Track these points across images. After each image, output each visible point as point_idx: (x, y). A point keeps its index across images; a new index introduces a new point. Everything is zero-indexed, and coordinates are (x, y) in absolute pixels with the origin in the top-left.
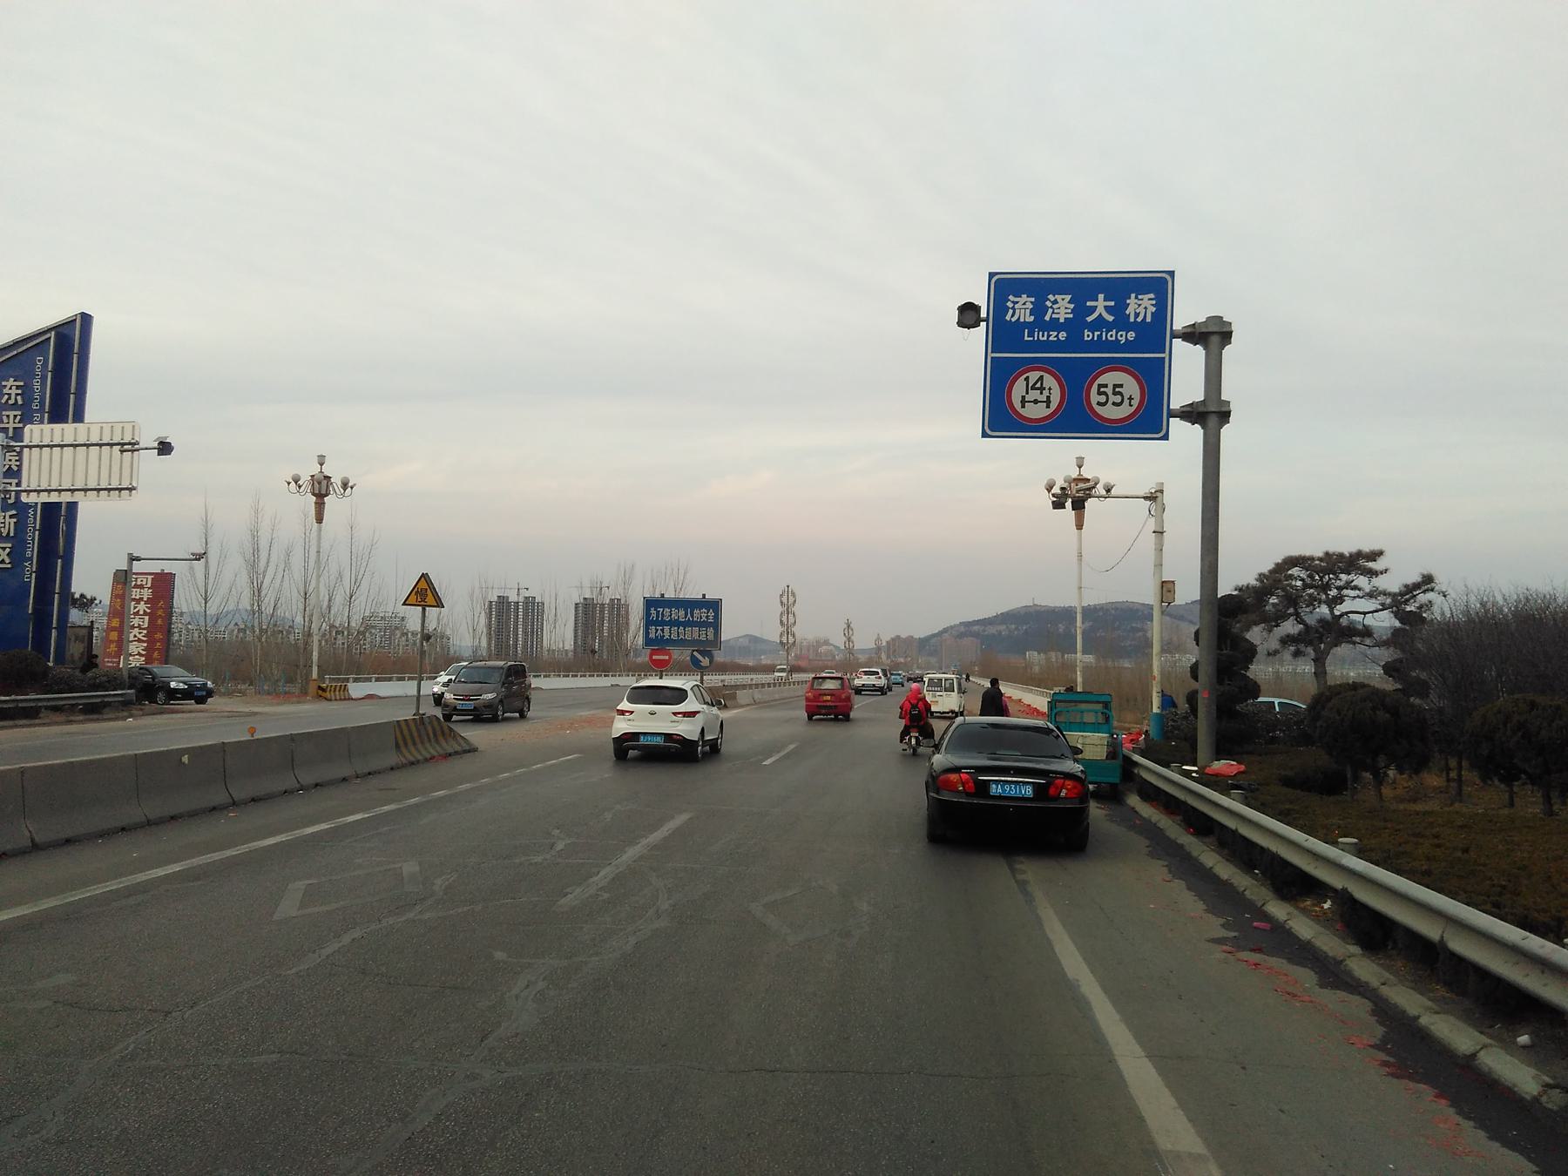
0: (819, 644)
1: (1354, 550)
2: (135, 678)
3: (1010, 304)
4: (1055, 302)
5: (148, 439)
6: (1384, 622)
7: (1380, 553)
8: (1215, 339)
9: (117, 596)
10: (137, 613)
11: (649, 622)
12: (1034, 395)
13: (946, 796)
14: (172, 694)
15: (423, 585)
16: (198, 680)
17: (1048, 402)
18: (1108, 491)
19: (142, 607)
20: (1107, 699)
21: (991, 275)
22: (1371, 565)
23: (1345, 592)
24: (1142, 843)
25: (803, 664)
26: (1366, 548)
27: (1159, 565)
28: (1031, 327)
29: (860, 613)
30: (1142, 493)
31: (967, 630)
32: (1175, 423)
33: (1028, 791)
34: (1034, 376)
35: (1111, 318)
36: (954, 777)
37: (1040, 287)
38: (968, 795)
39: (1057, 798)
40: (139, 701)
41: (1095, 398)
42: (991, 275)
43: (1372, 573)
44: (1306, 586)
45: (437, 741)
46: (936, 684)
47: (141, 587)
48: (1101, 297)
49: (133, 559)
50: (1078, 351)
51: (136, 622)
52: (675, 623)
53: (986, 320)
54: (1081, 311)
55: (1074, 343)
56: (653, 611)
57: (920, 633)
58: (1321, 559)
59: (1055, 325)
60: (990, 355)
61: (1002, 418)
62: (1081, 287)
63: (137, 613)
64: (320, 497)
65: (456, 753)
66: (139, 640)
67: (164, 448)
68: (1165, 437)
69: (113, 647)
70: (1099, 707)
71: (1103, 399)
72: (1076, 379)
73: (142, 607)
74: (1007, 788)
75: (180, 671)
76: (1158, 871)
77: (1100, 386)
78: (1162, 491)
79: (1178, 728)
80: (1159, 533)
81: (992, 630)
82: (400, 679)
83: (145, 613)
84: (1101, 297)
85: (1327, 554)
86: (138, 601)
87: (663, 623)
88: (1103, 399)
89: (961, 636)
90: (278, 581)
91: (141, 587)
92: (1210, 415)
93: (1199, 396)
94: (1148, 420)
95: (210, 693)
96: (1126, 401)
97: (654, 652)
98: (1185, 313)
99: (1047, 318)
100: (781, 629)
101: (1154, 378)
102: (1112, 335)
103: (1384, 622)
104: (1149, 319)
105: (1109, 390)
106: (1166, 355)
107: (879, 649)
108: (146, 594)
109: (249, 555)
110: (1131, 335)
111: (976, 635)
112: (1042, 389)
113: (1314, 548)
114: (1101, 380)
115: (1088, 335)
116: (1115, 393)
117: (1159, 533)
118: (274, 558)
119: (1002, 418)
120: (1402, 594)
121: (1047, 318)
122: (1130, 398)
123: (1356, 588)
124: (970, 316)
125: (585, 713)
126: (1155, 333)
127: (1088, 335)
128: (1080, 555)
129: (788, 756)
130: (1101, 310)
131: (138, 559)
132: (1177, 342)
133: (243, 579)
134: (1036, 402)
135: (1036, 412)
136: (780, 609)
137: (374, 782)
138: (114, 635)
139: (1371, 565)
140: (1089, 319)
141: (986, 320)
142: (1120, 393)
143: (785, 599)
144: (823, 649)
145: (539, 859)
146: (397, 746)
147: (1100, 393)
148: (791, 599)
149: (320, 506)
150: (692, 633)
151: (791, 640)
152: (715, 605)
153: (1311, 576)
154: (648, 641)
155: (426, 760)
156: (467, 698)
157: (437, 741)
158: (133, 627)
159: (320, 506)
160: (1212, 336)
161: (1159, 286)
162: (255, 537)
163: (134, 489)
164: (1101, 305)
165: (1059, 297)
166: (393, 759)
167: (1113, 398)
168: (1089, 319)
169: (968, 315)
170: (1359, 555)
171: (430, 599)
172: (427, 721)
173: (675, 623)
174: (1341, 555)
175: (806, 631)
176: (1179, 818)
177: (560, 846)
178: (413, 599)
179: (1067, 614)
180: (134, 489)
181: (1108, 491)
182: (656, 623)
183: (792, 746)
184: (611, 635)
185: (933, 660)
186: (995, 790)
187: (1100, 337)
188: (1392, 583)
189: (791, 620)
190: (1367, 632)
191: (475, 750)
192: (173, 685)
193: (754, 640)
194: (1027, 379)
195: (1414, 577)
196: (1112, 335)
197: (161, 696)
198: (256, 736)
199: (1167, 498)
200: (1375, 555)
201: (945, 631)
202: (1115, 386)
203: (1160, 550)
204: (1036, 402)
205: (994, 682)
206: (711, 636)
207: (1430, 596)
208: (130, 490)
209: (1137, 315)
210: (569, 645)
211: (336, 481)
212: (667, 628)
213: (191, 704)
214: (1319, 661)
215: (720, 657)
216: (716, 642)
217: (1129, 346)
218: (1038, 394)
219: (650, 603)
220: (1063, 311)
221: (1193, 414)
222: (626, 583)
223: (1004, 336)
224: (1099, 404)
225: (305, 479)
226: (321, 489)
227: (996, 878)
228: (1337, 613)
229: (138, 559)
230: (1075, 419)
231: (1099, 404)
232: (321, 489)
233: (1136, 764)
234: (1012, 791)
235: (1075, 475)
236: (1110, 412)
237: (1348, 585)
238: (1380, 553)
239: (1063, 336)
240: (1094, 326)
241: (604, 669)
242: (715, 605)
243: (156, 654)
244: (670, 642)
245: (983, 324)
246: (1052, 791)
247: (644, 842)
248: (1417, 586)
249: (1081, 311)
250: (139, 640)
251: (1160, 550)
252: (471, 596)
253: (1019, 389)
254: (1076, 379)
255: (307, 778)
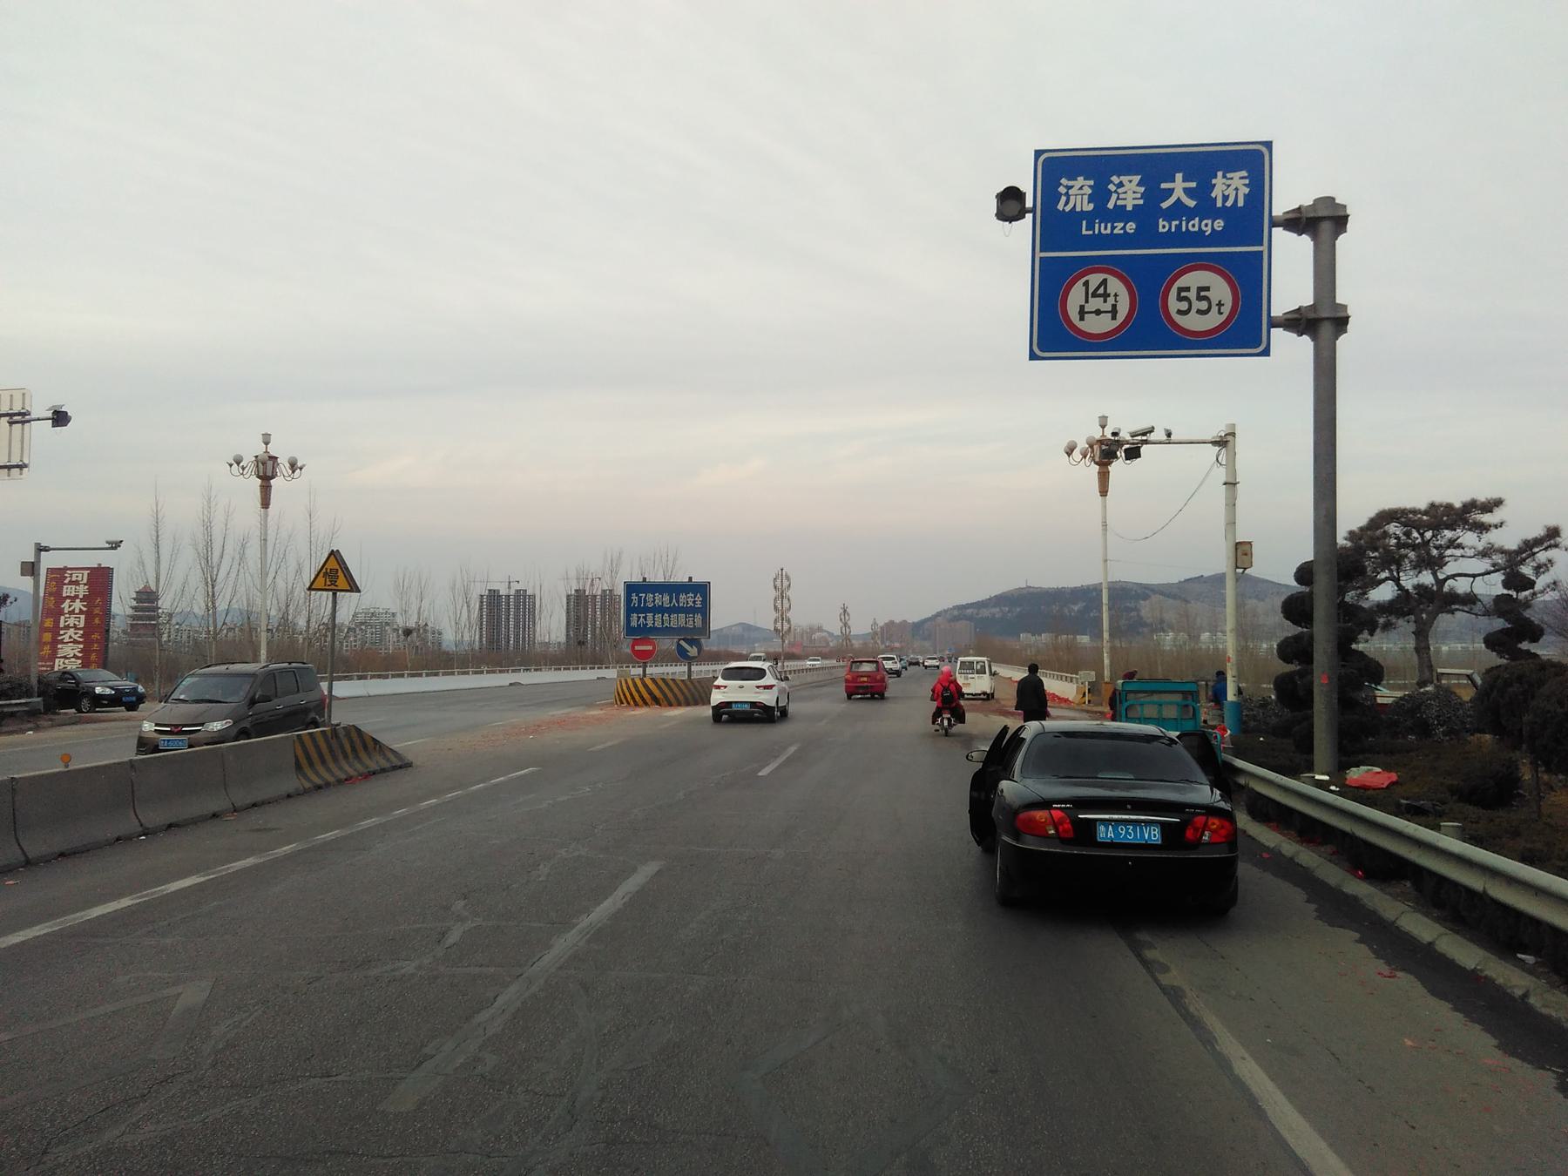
0: (812, 630)
1: (1467, 498)
2: (48, 684)
3: (1062, 190)
4: (1121, 185)
5: (40, 409)
6: (1492, 587)
7: (1498, 503)
8: (1326, 227)
9: (51, 594)
10: (72, 612)
11: (630, 610)
12: (1096, 303)
13: (1030, 844)
14: (98, 701)
15: (333, 564)
16: (126, 684)
17: (1114, 312)
18: (1169, 435)
19: (78, 605)
20: (1192, 687)
21: (1038, 153)
22: (1486, 518)
23: (1449, 552)
24: (1297, 895)
25: (795, 650)
26: (1482, 497)
27: (1231, 523)
28: (1090, 217)
29: (858, 598)
30: (1210, 438)
31: (960, 613)
32: (1278, 334)
33: (1153, 835)
34: (1095, 279)
35: (1191, 203)
36: (1040, 815)
37: (1100, 166)
38: (1064, 841)
39: (1197, 844)
40: (49, 709)
41: (1174, 305)
42: (1038, 153)
43: (1482, 528)
44: (1400, 545)
45: (357, 757)
46: (968, 666)
47: (76, 583)
48: (1179, 176)
49: (40, 549)
50: (1150, 249)
51: (71, 621)
52: (660, 610)
53: (1033, 210)
54: (1154, 195)
55: (1147, 235)
56: (634, 597)
57: (914, 617)
58: (1426, 513)
59: (1121, 214)
60: (1039, 255)
61: (1054, 335)
62: (1153, 165)
63: (72, 612)
64: (266, 479)
65: (383, 770)
66: (75, 642)
67: (60, 418)
68: (1266, 353)
69: (47, 650)
70: (1178, 698)
71: (1184, 306)
72: (1149, 282)
73: (78, 605)
74: (1122, 830)
75: (112, 676)
76: (1348, 946)
77: (1180, 290)
78: (1233, 434)
79: (1254, 718)
80: (1231, 484)
81: (985, 613)
82: (360, 678)
83: (81, 612)
84: (1179, 176)
85: (1432, 505)
86: (73, 599)
87: (646, 610)
88: (1184, 306)
89: (956, 619)
90: (233, 575)
91: (76, 583)
92: (1322, 322)
93: (1307, 299)
94: (1243, 332)
95: (141, 699)
96: (1215, 309)
97: (636, 642)
98: (1287, 195)
99: (1111, 205)
100: (774, 615)
101: (1249, 278)
102: (1194, 225)
103: (1492, 587)
104: (1241, 203)
105: (1192, 295)
106: (1264, 248)
107: (875, 633)
108: (82, 590)
109: (201, 546)
110: (1219, 224)
111: (970, 618)
112: (1106, 296)
113: (1417, 498)
114: (1182, 282)
115: (1163, 226)
116: (1200, 298)
117: (1231, 484)
118: (229, 550)
119: (1054, 335)
120: (1520, 551)
121: (1111, 205)
122: (1220, 304)
123: (1460, 546)
124: (1013, 207)
125: (558, 712)
126: (1249, 221)
127: (1163, 226)
128: (1105, 525)
129: (789, 761)
130: (1179, 193)
131: (46, 549)
132: (1278, 232)
133: (196, 579)
134: (1098, 312)
135: (1098, 325)
136: (774, 593)
137: (256, 818)
138: (47, 637)
139: (1486, 518)
140: (1165, 205)
141: (1033, 210)
142: (1206, 298)
143: (778, 582)
144: (817, 635)
145: (409, 967)
146: (298, 767)
147: (1180, 299)
148: (786, 583)
149: (266, 491)
150: (678, 620)
151: (786, 626)
152: (702, 589)
153: (1408, 534)
154: (630, 631)
155: (340, 782)
156: (176, 730)
157: (357, 757)
158: (67, 627)
159: (266, 491)
160: (1322, 222)
161: (1252, 161)
162: (208, 527)
163: (26, 466)
164: (1179, 187)
165: (1124, 179)
166: (292, 783)
167: (1197, 305)
168: (1165, 205)
169: (1010, 203)
170: (1471, 506)
171: (342, 582)
172: (342, 734)
173: (660, 610)
174: (1449, 507)
175: (800, 618)
176: (1329, 848)
177: (453, 937)
178: (320, 582)
179: (1096, 589)
180: (26, 466)
181: (1169, 435)
182: (638, 610)
183: (792, 749)
184: (603, 625)
185: (927, 644)
186: (1105, 834)
187: (1179, 227)
188: (1508, 539)
189: (786, 605)
190: (1470, 600)
191: (409, 765)
192: (98, 690)
193: (748, 628)
194: (1086, 284)
195: (1538, 532)
196: (1194, 225)
197: (85, 703)
198: (75, 765)
199: (1241, 444)
200: (1491, 506)
201: (938, 614)
202: (1200, 289)
203: (1231, 504)
204: (1098, 312)
205: (1033, 669)
206: (699, 623)
207: (1552, 553)
208: (21, 467)
209: (1226, 198)
210: (563, 639)
211: (283, 462)
212: (650, 615)
213: (121, 712)
214: (1422, 634)
215: (710, 645)
216: (705, 629)
217: (1216, 238)
218: (1101, 303)
219: (631, 588)
220: (1130, 195)
221: (1300, 322)
222: (614, 572)
223: (1056, 230)
224: (1180, 312)
225: (248, 460)
226: (266, 470)
227: (1105, 956)
228: (1441, 577)
229: (46, 549)
230: (1148, 333)
231: (1180, 312)
232: (266, 470)
233: (1240, 771)
234: (1129, 835)
235: (1098, 436)
236: (1194, 323)
237: (1452, 544)
238: (1498, 503)
239: (1131, 227)
240: (1170, 214)
241: (597, 661)
242: (702, 589)
243: (93, 656)
244: (654, 630)
245: (1029, 216)
246: (1189, 834)
247: (585, 922)
248: (1538, 542)
249: (1154, 195)
250: (75, 642)
251: (1231, 504)
252: (453, 588)
253: (1076, 297)
254: (1149, 282)
255: (154, 816)
